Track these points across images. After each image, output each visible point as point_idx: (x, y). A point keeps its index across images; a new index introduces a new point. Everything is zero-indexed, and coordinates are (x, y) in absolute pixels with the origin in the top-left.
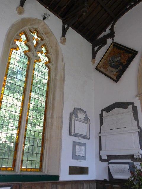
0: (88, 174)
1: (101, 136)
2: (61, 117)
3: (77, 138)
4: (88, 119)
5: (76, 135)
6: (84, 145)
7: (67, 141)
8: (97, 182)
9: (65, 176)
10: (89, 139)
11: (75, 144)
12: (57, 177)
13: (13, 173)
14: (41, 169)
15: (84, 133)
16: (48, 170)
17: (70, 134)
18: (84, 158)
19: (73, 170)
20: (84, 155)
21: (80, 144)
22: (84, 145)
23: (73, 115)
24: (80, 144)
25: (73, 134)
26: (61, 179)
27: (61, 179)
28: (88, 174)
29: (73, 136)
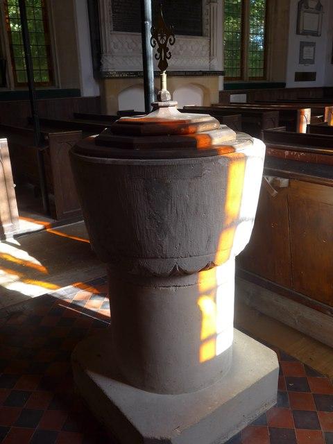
0: (296, 73)
1: (297, 74)
2: (288, 11)
3: (305, 37)
4: (321, 6)
5: (305, 33)
6: (313, 44)
7: (294, 41)
8: (325, 89)
9: (291, 83)
10: (320, 35)
11: (302, 45)
12: (284, 84)
13: (241, 82)
14: (241, 78)
15: (314, 29)
16: (273, 78)
17: (298, 32)
18: (312, 62)
19: (301, 77)
20: (312, 58)
21: (309, 44)
22: (313, 44)
23: (303, 5)
24: (309, 44)
25: (301, 32)
26: (288, 86)
27: (288, 86)
28: (296, 73)
29: (302, 34)
